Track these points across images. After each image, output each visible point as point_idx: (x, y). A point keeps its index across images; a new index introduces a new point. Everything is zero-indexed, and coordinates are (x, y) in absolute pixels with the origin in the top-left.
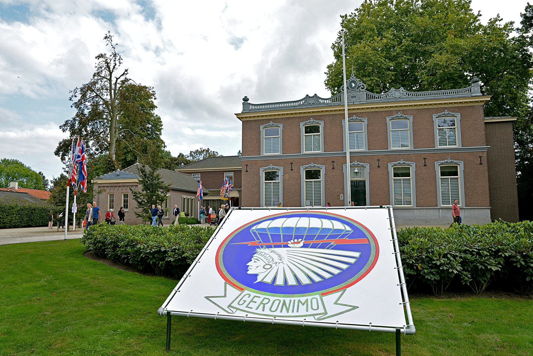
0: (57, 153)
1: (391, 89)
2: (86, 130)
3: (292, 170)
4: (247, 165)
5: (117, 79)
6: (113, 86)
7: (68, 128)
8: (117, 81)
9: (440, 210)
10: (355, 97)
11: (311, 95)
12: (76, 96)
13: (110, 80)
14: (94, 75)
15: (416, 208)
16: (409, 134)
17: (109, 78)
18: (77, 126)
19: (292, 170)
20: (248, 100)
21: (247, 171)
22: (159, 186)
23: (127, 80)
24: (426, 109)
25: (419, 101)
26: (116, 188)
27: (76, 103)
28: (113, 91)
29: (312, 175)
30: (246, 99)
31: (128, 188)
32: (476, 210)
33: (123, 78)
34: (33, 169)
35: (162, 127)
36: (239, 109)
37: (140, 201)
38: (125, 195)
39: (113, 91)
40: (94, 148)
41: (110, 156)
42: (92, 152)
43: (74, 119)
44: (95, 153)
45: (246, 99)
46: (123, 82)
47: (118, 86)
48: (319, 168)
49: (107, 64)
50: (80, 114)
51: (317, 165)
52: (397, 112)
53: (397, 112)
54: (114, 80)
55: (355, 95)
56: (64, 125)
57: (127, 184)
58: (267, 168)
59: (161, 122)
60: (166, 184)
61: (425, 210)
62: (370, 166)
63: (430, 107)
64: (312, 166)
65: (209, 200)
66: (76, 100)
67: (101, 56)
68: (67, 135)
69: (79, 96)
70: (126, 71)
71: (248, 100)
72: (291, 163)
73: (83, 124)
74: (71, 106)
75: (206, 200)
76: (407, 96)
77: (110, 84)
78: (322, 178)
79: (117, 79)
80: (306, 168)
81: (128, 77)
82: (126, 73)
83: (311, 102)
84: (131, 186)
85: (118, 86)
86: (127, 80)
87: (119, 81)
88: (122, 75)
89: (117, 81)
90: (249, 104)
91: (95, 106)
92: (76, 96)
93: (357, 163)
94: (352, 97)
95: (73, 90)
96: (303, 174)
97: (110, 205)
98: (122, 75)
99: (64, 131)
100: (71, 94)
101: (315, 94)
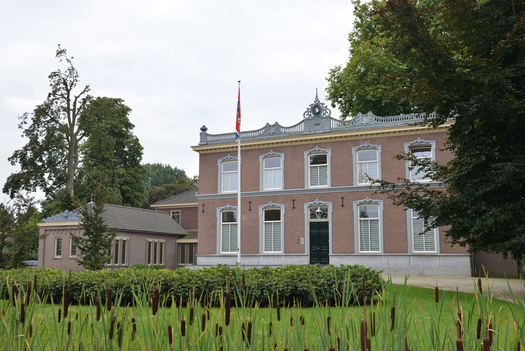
0: (5, 190)
1: (358, 115)
2: (41, 160)
3: (250, 210)
4: (203, 205)
5: (76, 98)
6: (72, 107)
7: (19, 159)
8: (76, 100)
9: (411, 258)
10: (319, 124)
11: (272, 123)
12: (25, 123)
13: (68, 100)
14: (50, 95)
15: (383, 254)
16: (378, 166)
17: (66, 96)
18: (29, 154)
19: (250, 210)
20: (206, 129)
21: (203, 212)
22: (103, 229)
23: (89, 97)
24: (397, 137)
25: (383, 128)
26: (64, 232)
27: (26, 130)
28: (71, 112)
29: (273, 215)
30: (204, 129)
31: (68, 233)
32: (453, 258)
33: (84, 96)
34: (351, 28)
35: (42, 190)
36: (196, 141)
37: (82, 247)
38: (58, 240)
39: (71, 112)
40: (51, 182)
41: (66, 191)
42: (48, 186)
43: (25, 149)
44: (53, 188)
45: (204, 129)
46: (85, 101)
47: (78, 105)
48: (279, 207)
49: (62, 84)
50: (34, 141)
51: (277, 205)
52: (364, 140)
53: (364, 140)
54: (72, 99)
55: (318, 122)
56: (12, 158)
57: (68, 228)
58: (224, 207)
59: (352, 52)
60: (111, 225)
61: (394, 257)
62: (333, 205)
63: (401, 134)
64: (272, 205)
65: (184, 244)
66: (26, 127)
67: (53, 75)
68: (17, 168)
69: (30, 122)
70: (87, 87)
71: (206, 129)
72: (250, 203)
73: (38, 154)
74: (22, 136)
75: (182, 243)
76: (376, 122)
77: (68, 104)
78: (282, 220)
79: (76, 98)
80: (265, 207)
81: (90, 93)
82: (87, 89)
83: (272, 131)
84: (71, 228)
85: (78, 105)
86: (89, 97)
87: (78, 99)
88: (82, 93)
89: (76, 100)
90: (207, 134)
91: (50, 131)
92: (25, 123)
93: (318, 202)
94: (316, 125)
95: (22, 115)
96: (262, 215)
97: (72, 251)
98: (82, 93)
99: (13, 164)
100: (21, 120)
101: (268, 124)
